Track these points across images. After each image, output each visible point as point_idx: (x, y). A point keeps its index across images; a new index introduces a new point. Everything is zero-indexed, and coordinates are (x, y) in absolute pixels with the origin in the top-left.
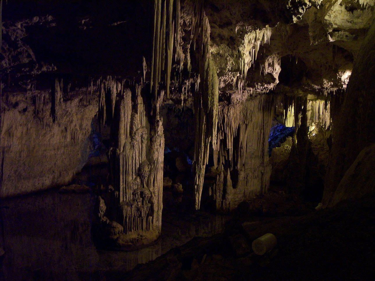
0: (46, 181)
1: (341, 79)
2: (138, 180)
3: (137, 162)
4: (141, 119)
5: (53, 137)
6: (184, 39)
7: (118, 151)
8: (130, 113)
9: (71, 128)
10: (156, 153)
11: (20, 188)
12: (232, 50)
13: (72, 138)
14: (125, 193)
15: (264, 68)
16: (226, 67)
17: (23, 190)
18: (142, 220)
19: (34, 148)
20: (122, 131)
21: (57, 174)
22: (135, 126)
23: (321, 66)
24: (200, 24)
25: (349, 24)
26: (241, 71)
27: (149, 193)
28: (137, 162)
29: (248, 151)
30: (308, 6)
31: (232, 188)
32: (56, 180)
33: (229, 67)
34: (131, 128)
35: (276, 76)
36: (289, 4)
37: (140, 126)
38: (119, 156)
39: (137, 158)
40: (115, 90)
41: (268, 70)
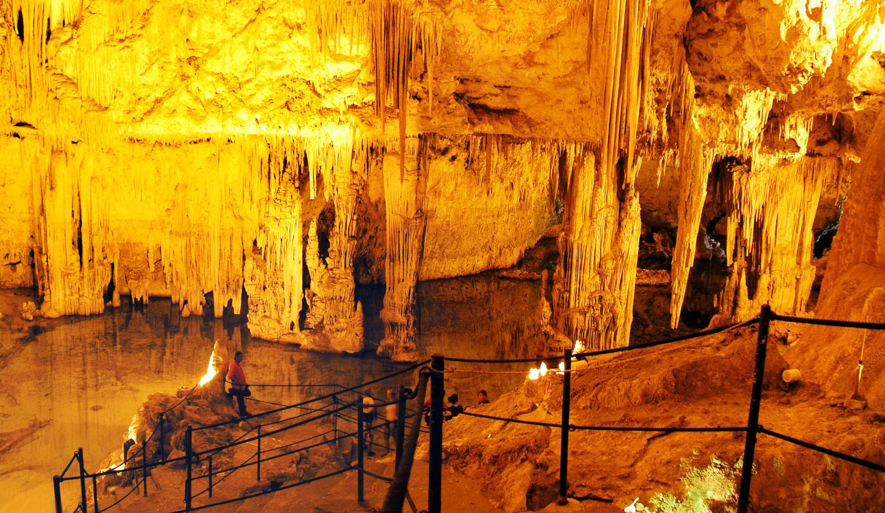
2: (598, 279)
3: (598, 254)
4: (607, 195)
6: (658, 101)
7: (572, 238)
8: (591, 186)
10: (626, 242)
11: (442, 270)
13: (520, 199)
15: (783, 131)
16: (718, 137)
17: (446, 273)
18: (600, 335)
19: (464, 213)
20: (578, 210)
21: (495, 252)
24: (679, 82)
26: (737, 143)
27: (612, 299)
28: (598, 254)
29: (778, 243)
31: (747, 298)
32: (493, 261)
33: (722, 137)
34: (592, 207)
36: (786, 69)
37: (604, 204)
39: (598, 249)
40: (573, 153)
41: (788, 134)
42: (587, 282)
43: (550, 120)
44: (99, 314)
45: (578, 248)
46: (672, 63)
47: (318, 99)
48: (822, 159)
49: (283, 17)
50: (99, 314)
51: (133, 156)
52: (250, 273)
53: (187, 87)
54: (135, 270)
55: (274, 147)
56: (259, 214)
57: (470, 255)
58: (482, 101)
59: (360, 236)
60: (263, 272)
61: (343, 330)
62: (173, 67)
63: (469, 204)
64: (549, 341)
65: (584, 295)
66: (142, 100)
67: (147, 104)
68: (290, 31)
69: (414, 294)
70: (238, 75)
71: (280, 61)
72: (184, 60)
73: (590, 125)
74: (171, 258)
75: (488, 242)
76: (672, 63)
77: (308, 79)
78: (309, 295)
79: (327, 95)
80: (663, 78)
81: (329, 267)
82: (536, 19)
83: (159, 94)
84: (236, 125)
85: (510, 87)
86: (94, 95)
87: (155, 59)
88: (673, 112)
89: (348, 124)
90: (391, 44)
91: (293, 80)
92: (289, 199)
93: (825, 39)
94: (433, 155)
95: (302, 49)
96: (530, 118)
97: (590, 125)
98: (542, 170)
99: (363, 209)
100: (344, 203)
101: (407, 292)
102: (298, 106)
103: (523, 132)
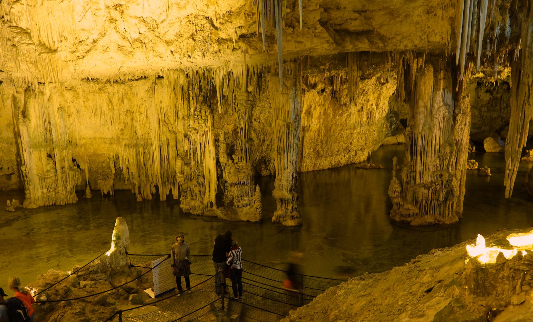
0: (342, 160)
2: (438, 161)
3: (438, 142)
5: (350, 116)
7: (416, 132)
9: (367, 108)
13: (368, 118)
21: (353, 153)
28: (438, 142)
32: (351, 159)
38: (416, 135)
42: (430, 164)
43: (400, 34)
44: (73, 203)
50: (73, 203)
51: (89, 91)
52: (180, 169)
53: (115, 28)
54: (102, 174)
55: (191, 77)
56: (184, 127)
57: (337, 155)
58: (344, 26)
59: (261, 144)
60: (189, 168)
62: (103, 12)
64: (400, 210)
66: (83, 42)
67: (87, 45)
69: (296, 177)
70: (156, 19)
72: (111, 7)
73: (436, 31)
74: (127, 163)
75: (348, 146)
78: (222, 182)
79: (222, 27)
81: (235, 161)
83: (95, 37)
84: (157, 56)
85: (366, 11)
86: (45, 40)
87: (88, 7)
88: (518, 8)
89: (240, 51)
91: (196, 17)
92: (203, 114)
94: (306, 88)
96: (383, 35)
97: (436, 31)
98: (382, 98)
99: (262, 126)
100: (243, 114)
101: (291, 176)
102: (201, 37)
103: (378, 48)
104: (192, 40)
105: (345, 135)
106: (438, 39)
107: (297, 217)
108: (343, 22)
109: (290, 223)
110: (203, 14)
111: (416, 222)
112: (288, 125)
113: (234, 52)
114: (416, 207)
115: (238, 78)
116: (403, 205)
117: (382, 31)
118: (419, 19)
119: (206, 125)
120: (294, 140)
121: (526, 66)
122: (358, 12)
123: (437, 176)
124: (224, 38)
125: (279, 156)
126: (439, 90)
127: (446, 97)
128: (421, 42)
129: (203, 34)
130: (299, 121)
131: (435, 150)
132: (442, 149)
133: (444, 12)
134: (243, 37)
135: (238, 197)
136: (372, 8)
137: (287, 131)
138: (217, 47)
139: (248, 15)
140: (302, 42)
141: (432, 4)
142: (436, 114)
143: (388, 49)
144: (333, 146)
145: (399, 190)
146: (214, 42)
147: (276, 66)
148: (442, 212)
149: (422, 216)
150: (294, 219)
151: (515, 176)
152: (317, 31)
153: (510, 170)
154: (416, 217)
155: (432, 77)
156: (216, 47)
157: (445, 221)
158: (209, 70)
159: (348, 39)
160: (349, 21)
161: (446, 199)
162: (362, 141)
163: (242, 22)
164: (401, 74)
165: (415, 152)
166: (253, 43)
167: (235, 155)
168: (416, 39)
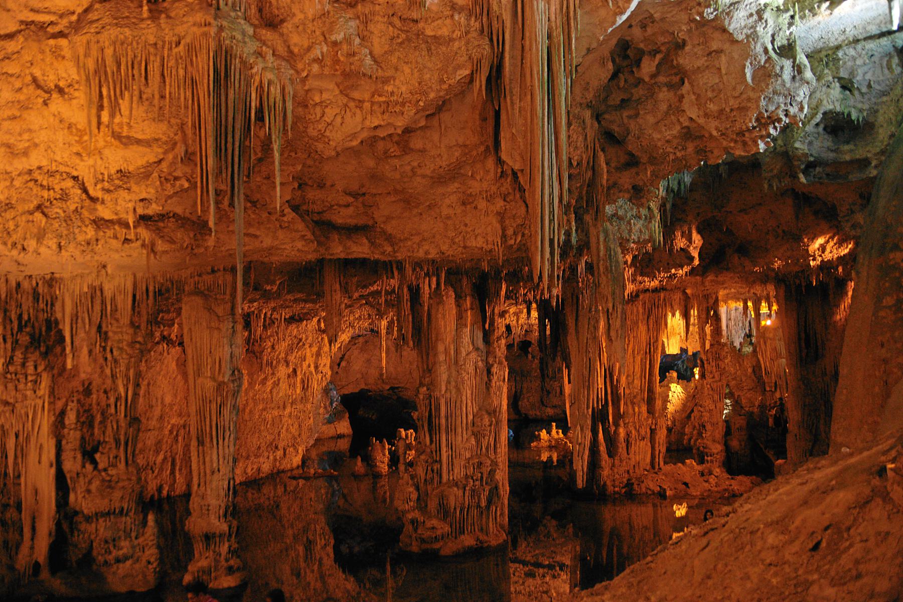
0: (265, 465)
1: (807, 251)
2: (473, 441)
5: (278, 385)
8: (454, 327)
9: (302, 370)
12: (638, 208)
14: (451, 464)
21: (279, 453)
22: (464, 347)
23: (767, 233)
25: (832, 155)
30: (783, 123)
32: (278, 463)
35: (695, 254)
36: (753, 121)
38: (438, 399)
40: (427, 288)
42: (461, 446)
43: (418, 234)
45: (446, 403)
46: (586, 139)
47: (92, 204)
48: (667, 293)
49: (32, 75)
58: (327, 216)
61: (126, 558)
63: (251, 394)
64: (419, 531)
65: (459, 464)
68: (47, 96)
71: (27, 145)
75: (274, 439)
76: (586, 139)
77: (75, 174)
79: (107, 197)
80: (576, 158)
81: (101, 466)
82: (428, 76)
89: (139, 243)
90: (223, 105)
91: (51, 174)
92: (30, 369)
93: (802, 79)
95: (67, 125)
96: (390, 235)
101: (226, 487)
103: (383, 253)
104: (41, 215)
105: (270, 419)
106: (481, 243)
107: (238, 569)
108: (325, 209)
109: (228, 582)
110: (67, 170)
111: (448, 548)
112: (220, 386)
113: (126, 245)
114: (446, 522)
115: (113, 299)
116: (424, 522)
117: (389, 229)
118: (451, 212)
119: (35, 392)
120: (232, 416)
121: (602, 286)
122: (350, 194)
123: (473, 464)
124: (107, 217)
125: (201, 447)
126: (466, 326)
127: (475, 338)
128: (451, 247)
129: (64, 206)
130: (239, 379)
131: (467, 424)
132: (477, 420)
133: (488, 204)
134: (144, 219)
135: (106, 542)
136: (374, 191)
137: (219, 399)
138: (93, 233)
139: (166, 179)
140: (256, 237)
141: (471, 190)
142: (464, 364)
143: (400, 256)
144: (249, 440)
145: (414, 496)
146: (87, 223)
147: (196, 278)
148: (484, 528)
149: (456, 538)
150: (234, 572)
151: (587, 452)
152: (285, 219)
153: (580, 444)
154: (447, 541)
155: (454, 306)
156: (90, 232)
157: (490, 542)
158: (51, 281)
159: (336, 236)
160: (335, 207)
161: (489, 502)
162: (294, 430)
163: (152, 191)
164: (407, 300)
165: (437, 428)
166: (166, 230)
167: (102, 453)
168: (444, 242)
